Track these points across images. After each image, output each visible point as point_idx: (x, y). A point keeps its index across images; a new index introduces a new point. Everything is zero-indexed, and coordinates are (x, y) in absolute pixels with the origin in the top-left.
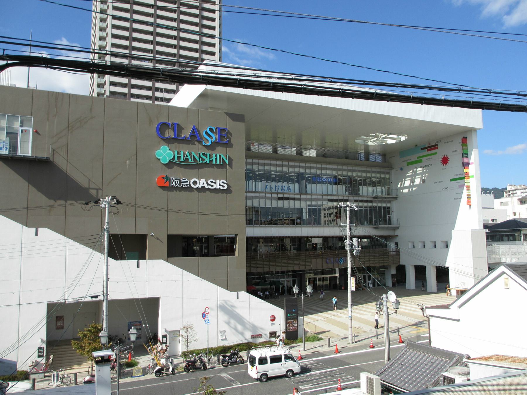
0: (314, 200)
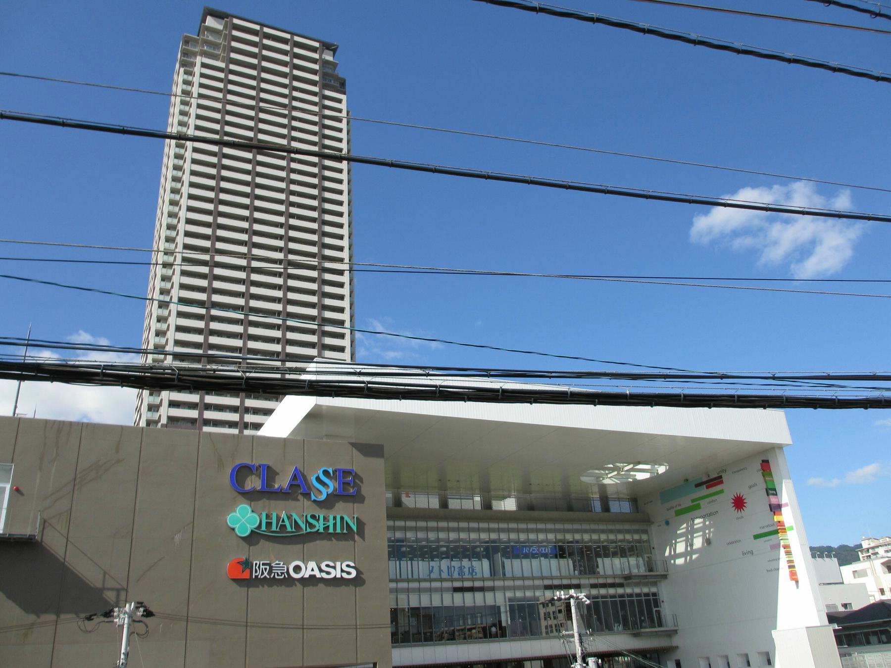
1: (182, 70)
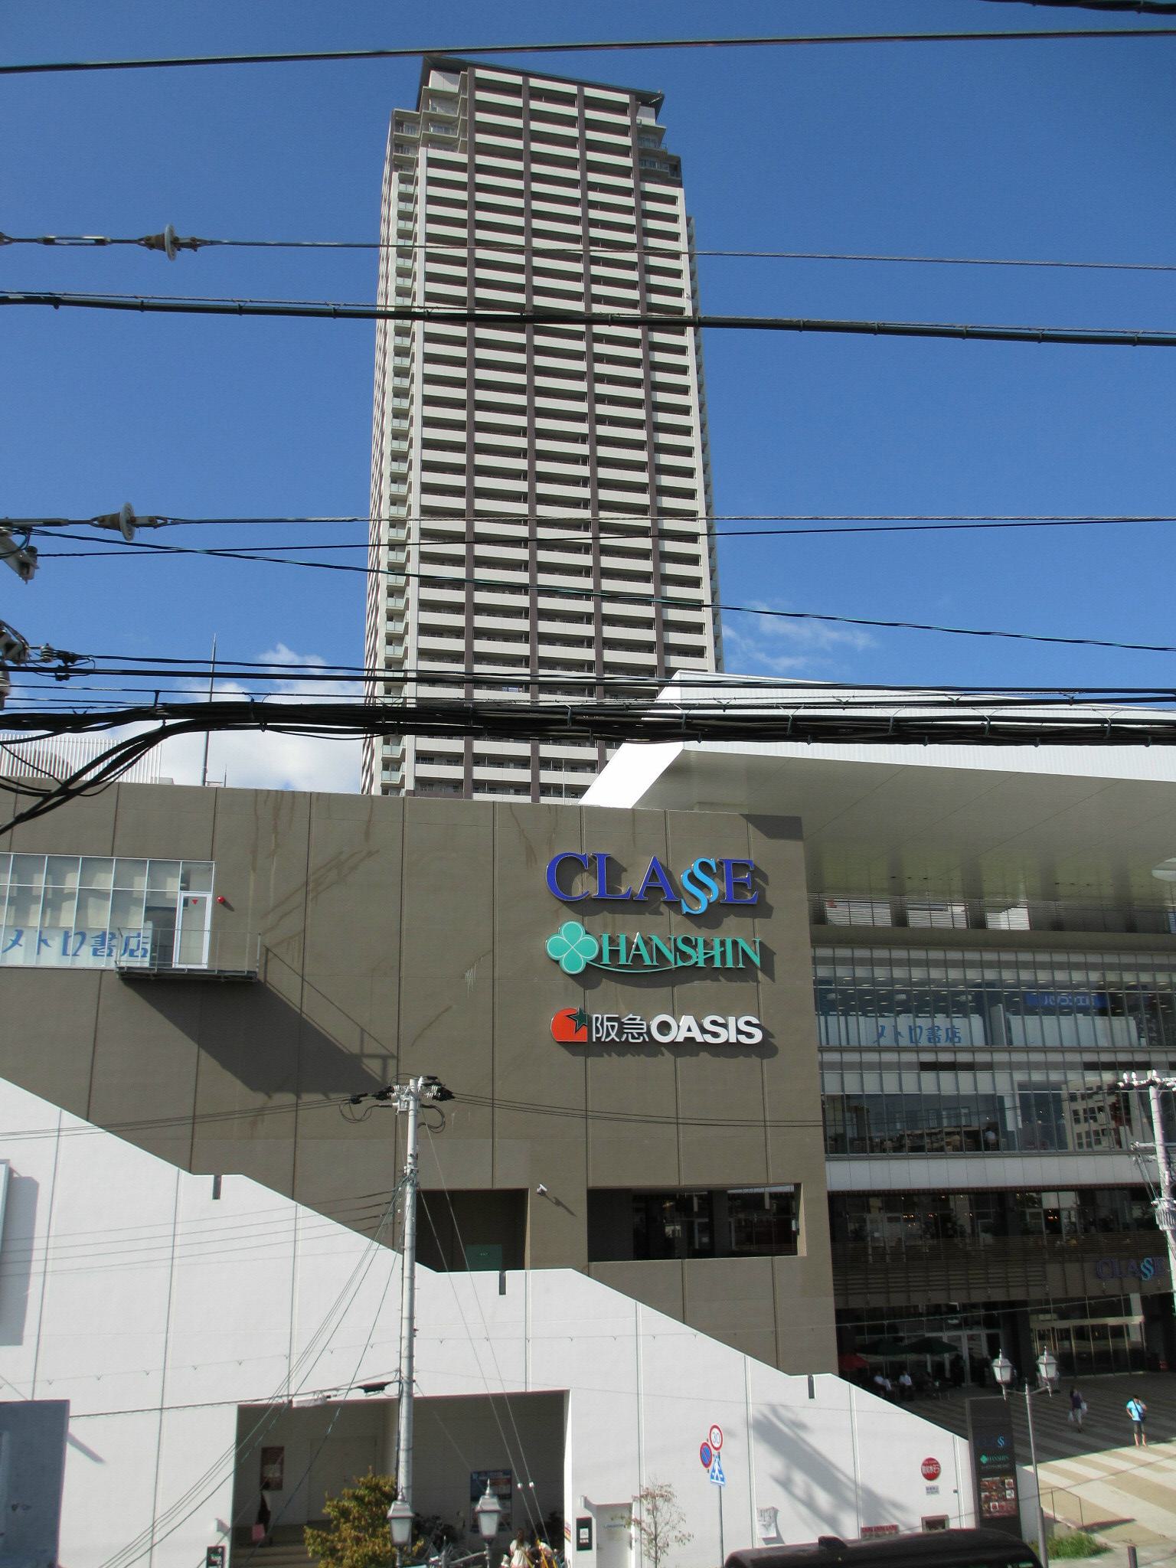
0: (1037, 1066)
1: (395, 175)
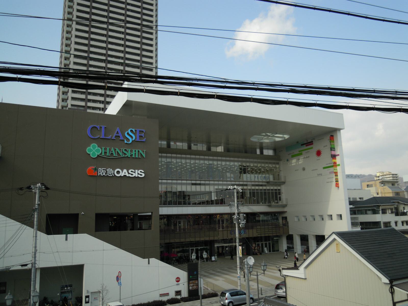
0: (220, 185)
